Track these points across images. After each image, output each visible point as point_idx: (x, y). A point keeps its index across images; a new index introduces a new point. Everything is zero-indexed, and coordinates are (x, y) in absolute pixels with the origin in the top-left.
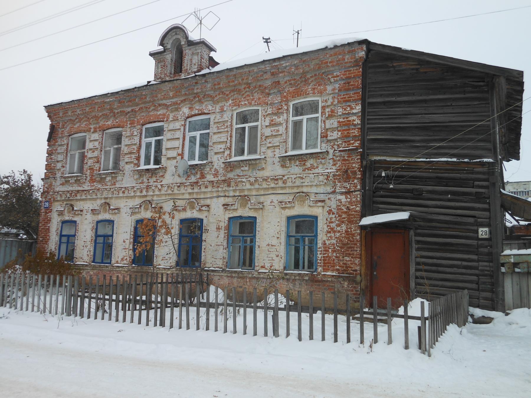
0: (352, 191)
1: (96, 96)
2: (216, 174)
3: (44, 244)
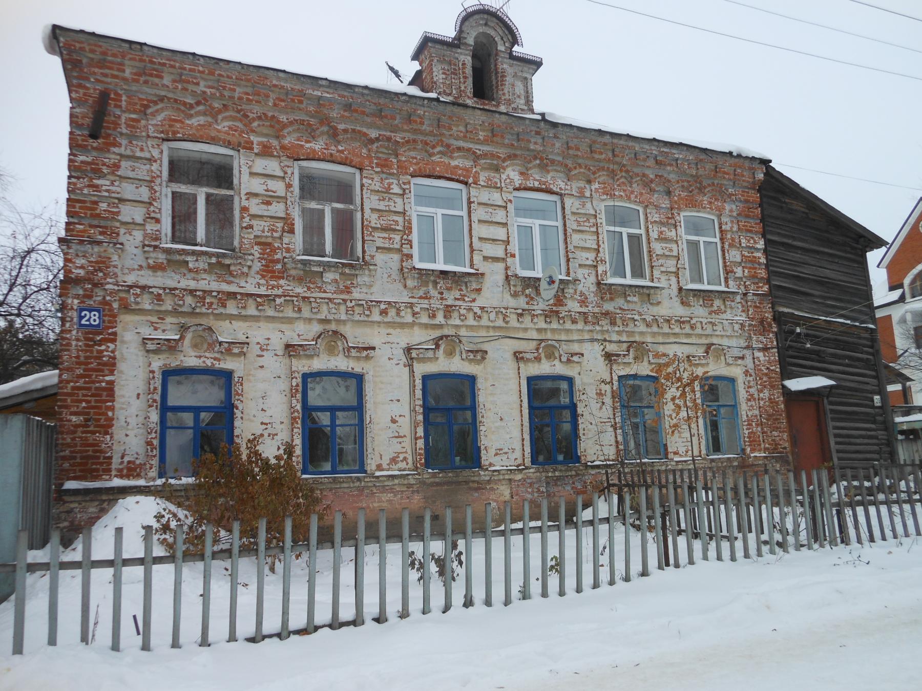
0: (769, 348)
1: (284, 71)
2: (583, 302)
3: (94, 433)
